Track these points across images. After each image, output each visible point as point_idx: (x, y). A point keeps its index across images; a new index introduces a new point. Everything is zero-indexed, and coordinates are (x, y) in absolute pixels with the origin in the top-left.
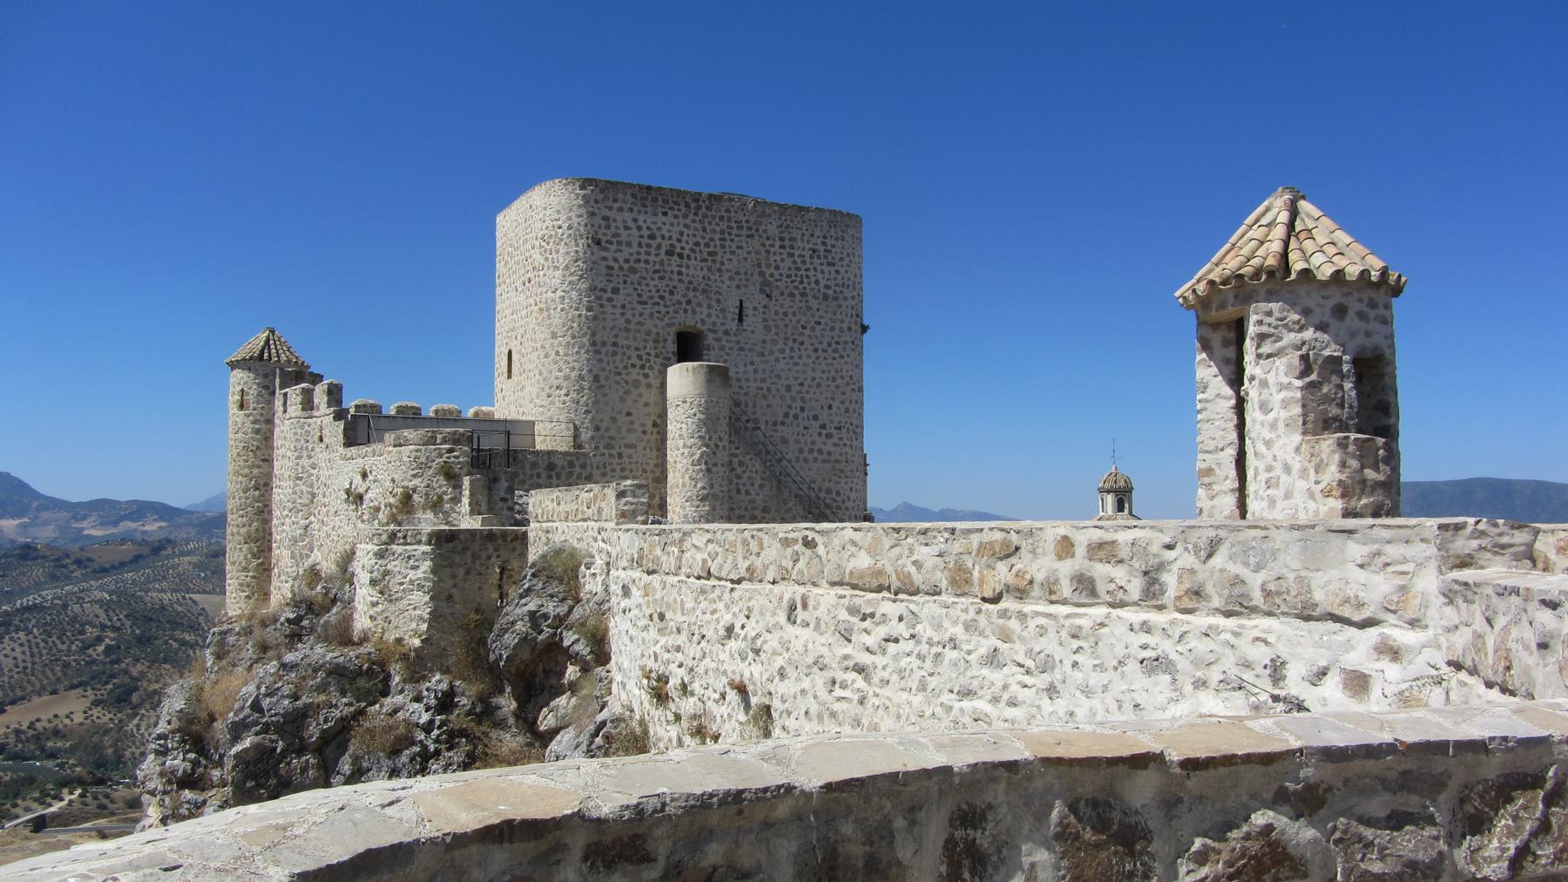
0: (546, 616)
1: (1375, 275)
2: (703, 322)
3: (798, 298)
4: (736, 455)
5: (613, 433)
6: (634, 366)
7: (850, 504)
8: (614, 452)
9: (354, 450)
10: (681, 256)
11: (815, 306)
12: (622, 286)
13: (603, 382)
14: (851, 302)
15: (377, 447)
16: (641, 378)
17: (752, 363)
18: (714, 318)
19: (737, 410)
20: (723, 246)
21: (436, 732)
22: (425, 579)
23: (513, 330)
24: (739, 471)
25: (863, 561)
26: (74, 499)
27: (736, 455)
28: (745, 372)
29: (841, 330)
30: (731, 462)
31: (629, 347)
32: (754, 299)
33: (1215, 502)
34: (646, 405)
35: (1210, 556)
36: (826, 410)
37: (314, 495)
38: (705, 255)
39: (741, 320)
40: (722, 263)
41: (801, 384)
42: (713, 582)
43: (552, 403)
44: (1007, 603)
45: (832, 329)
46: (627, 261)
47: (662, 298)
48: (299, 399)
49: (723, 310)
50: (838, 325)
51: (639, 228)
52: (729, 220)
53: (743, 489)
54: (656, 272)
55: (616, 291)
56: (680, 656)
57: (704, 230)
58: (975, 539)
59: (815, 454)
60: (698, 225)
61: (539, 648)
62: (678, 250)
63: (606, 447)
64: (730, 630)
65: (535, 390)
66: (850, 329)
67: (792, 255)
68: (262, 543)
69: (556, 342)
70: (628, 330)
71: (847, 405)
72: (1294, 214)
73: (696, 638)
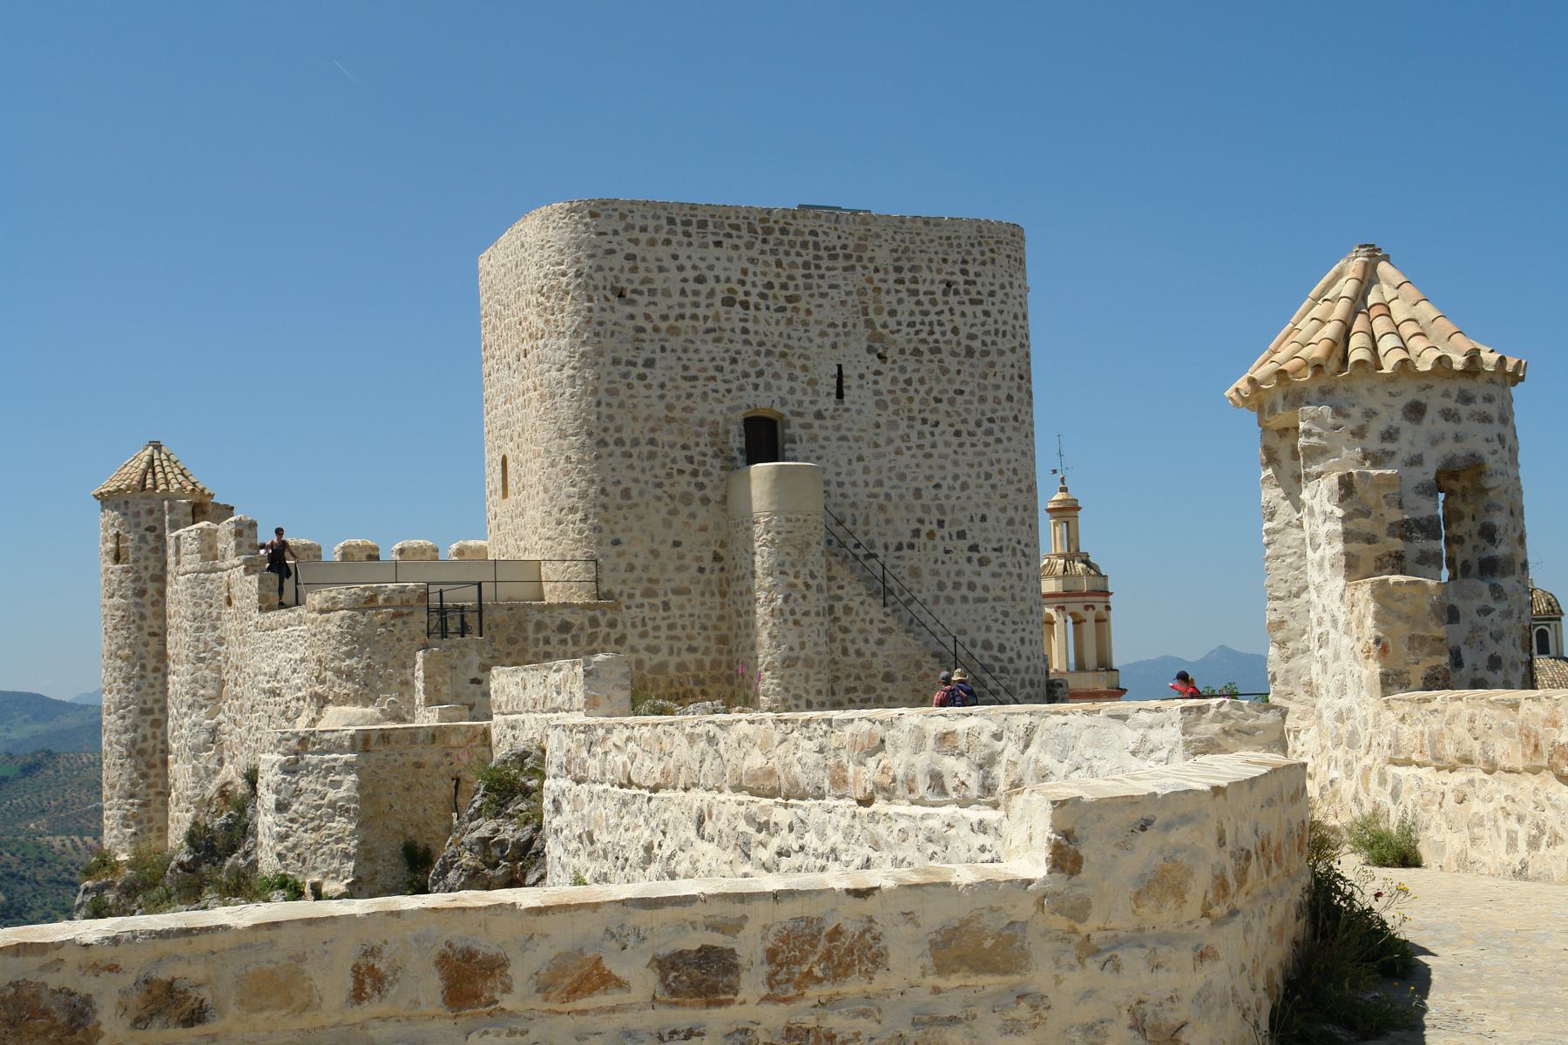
0: (502, 844)
1: (1459, 361)
2: (783, 402)
3: (927, 356)
4: (840, 598)
5: (654, 572)
6: (681, 472)
7: (1022, 664)
8: (658, 601)
10: (745, 305)
11: (953, 368)
12: (658, 355)
13: (636, 499)
14: (1010, 358)
16: (692, 489)
17: (860, 459)
18: (798, 396)
19: (839, 530)
20: (808, 287)
22: (349, 799)
23: (507, 426)
24: (845, 621)
25: (756, 761)
27: (840, 598)
28: (850, 473)
29: (997, 401)
30: (831, 608)
31: (672, 446)
32: (858, 361)
33: (1291, 664)
34: (703, 529)
35: (1027, 746)
36: (977, 524)
37: (223, 683)
38: (782, 302)
39: (840, 395)
41: (937, 486)
42: (634, 791)
43: (564, 533)
44: (880, 806)
45: (982, 400)
46: (665, 318)
47: (720, 369)
49: (812, 382)
50: (990, 394)
51: (681, 268)
52: (816, 246)
53: (852, 649)
54: (708, 331)
55: (649, 363)
57: (779, 264)
58: (849, 729)
59: (964, 591)
60: (771, 259)
62: (740, 297)
63: (643, 595)
64: (648, 848)
65: (539, 516)
66: (1010, 398)
67: (914, 293)
68: (150, 759)
69: (565, 443)
70: (670, 420)
71: (1011, 513)
72: (1368, 279)
73: (621, 861)
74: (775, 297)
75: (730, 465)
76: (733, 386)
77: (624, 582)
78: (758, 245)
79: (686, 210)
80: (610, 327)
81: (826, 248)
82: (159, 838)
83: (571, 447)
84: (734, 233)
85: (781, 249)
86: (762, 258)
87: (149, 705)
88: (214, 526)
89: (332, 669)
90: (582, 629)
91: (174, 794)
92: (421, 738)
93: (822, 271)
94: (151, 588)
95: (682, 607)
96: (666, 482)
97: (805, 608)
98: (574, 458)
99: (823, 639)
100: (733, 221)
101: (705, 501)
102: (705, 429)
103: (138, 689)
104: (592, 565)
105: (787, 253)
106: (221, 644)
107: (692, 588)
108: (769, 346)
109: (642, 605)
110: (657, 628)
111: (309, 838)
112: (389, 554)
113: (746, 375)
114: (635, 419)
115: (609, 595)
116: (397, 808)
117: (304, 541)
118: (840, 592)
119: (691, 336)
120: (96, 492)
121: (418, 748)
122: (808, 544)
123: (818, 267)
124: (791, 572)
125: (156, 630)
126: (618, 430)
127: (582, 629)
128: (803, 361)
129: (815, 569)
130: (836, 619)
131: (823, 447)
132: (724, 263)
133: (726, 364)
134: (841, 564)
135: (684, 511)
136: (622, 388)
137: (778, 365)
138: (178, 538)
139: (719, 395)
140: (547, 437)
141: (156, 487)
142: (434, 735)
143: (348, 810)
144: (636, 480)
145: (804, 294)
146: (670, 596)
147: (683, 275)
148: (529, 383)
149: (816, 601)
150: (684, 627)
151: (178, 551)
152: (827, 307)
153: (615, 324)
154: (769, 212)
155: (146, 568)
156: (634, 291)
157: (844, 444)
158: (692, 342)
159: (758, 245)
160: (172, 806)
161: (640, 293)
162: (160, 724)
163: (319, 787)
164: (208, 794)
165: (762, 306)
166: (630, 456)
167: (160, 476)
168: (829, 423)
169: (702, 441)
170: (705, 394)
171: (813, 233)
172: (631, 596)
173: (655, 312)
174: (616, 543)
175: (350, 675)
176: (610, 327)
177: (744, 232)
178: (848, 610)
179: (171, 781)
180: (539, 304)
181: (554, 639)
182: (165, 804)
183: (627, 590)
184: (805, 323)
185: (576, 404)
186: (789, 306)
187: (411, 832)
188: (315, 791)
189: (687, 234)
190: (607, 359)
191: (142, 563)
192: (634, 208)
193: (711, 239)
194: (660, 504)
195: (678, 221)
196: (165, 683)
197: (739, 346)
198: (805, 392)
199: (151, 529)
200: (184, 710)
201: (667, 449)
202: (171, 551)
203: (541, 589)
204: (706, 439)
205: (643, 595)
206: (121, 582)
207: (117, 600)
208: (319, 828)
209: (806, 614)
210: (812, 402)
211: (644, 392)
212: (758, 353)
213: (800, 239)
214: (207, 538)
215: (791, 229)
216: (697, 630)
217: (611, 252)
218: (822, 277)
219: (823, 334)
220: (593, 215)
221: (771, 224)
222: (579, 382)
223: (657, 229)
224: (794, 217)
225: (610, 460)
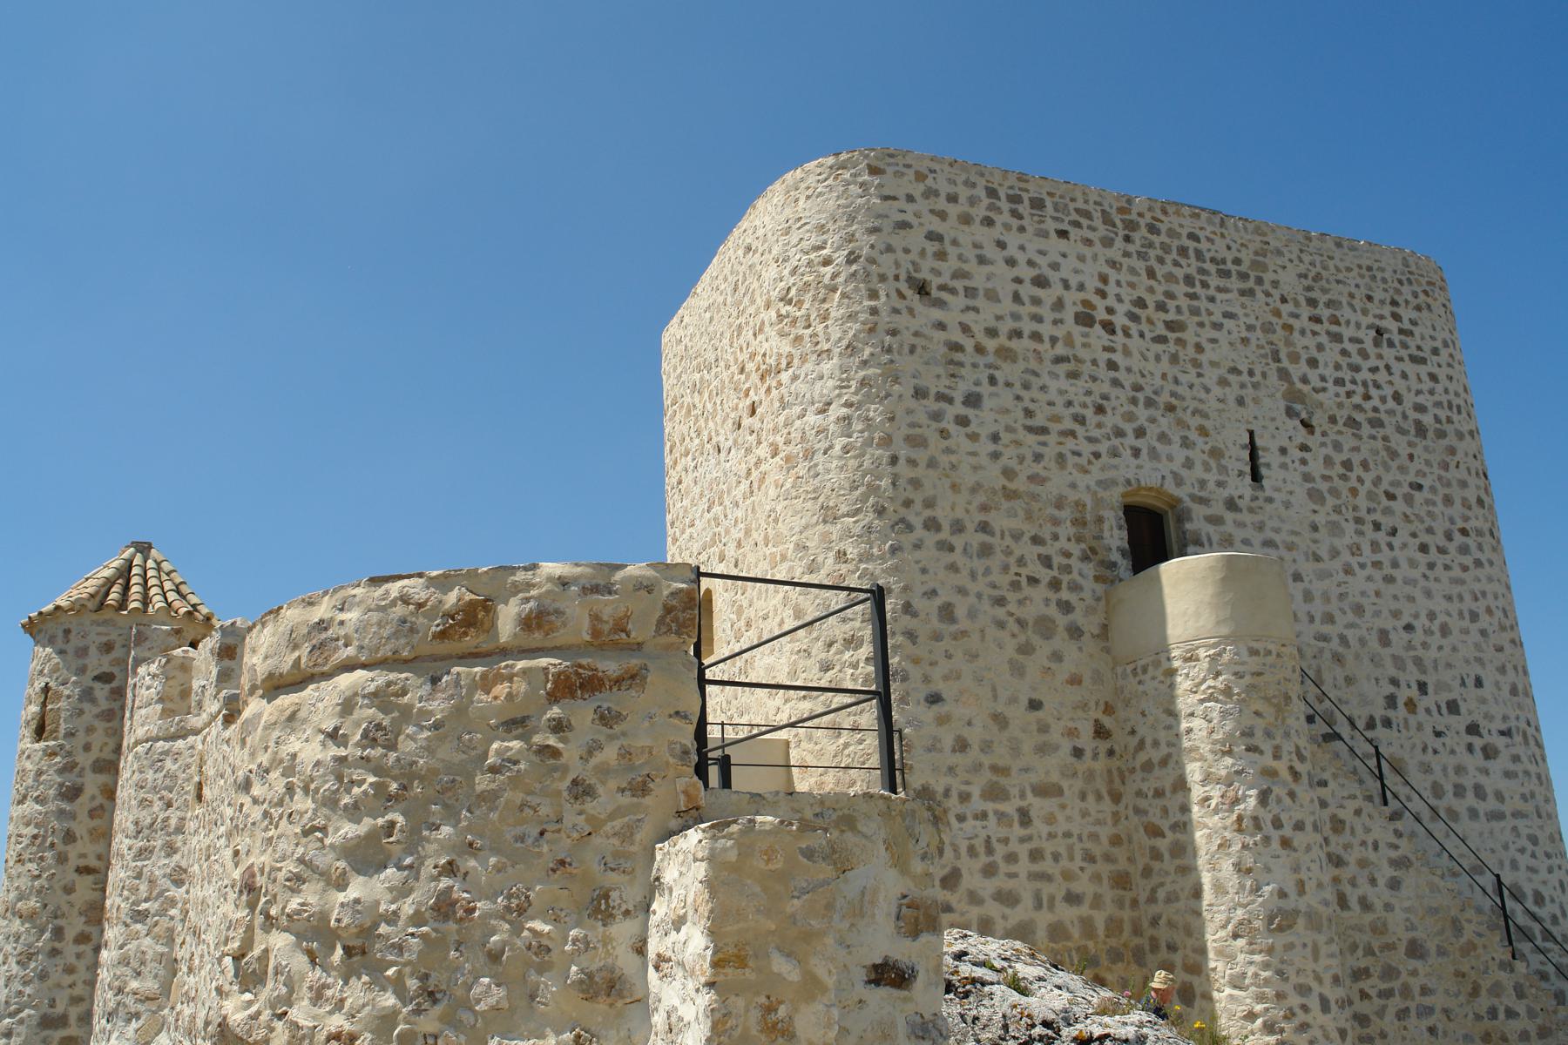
5: (1001, 756)
8: (1009, 808)
10: (1109, 327)
12: (985, 389)
13: (964, 624)
16: (1053, 611)
20: (1195, 312)
31: (1017, 536)
34: (1075, 680)
37: (172, 966)
38: (1161, 330)
46: (992, 333)
51: (1011, 262)
54: (1058, 360)
55: (973, 400)
57: (1151, 274)
62: (1101, 315)
69: (835, 530)
75: (1107, 575)
78: (1119, 243)
83: (847, 534)
85: (1152, 253)
86: (1126, 261)
87: (60, 1009)
94: (92, 784)
95: (1050, 819)
96: (1012, 597)
97: (1298, 816)
98: (852, 552)
100: (1080, 204)
101: (1075, 632)
102: (1066, 514)
103: (43, 976)
105: (1161, 260)
106: (178, 883)
107: (1065, 784)
109: (983, 816)
110: (1011, 858)
119: (1033, 365)
123: (1205, 285)
124: (1267, 747)
125: (93, 862)
126: (929, 503)
133: (1089, 413)
135: (1043, 649)
137: (1165, 423)
139: (1083, 461)
140: (798, 523)
144: (962, 591)
152: (1224, 342)
153: (916, 334)
156: (942, 288)
159: (1119, 243)
161: (953, 291)
166: (951, 549)
171: (1193, 237)
172: (965, 797)
173: (978, 323)
175: (359, 950)
183: (957, 786)
184: (1196, 364)
185: (853, 463)
186: (1171, 336)
189: (1016, 214)
190: (904, 389)
191: (82, 737)
192: (937, 167)
193: (1051, 226)
194: (1003, 635)
197: (1106, 388)
198: (1207, 469)
199: (105, 678)
201: (1008, 541)
204: (1067, 530)
206: (39, 773)
207: (30, 807)
209: (1299, 826)
211: (967, 445)
215: (1163, 228)
216: (1078, 862)
217: (904, 225)
221: (1134, 216)
222: (858, 426)
225: (918, 554)
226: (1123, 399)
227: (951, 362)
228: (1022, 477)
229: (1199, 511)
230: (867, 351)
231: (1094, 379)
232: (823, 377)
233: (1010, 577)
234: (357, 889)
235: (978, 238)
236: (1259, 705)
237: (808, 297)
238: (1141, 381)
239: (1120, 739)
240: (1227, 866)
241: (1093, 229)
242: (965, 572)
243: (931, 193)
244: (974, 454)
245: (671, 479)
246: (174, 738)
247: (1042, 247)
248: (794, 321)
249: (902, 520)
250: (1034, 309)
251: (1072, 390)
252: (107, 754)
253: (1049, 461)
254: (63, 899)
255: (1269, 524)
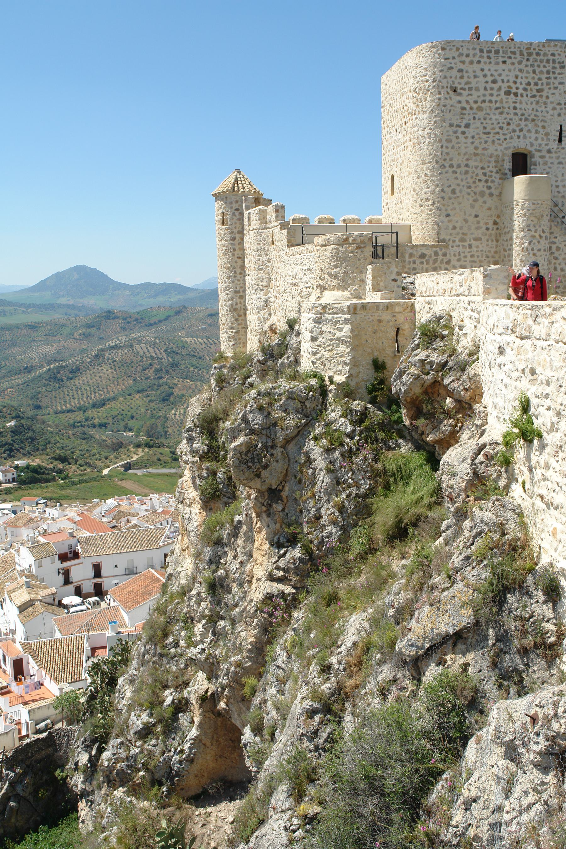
0: (431, 363)
2: (532, 144)
4: (555, 243)
5: (465, 230)
8: (466, 244)
9: (294, 249)
10: (516, 95)
12: (472, 121)
13: (458, 194)
15: (310, 247)
16: (485, 189)
20: (548, 84)
21: (357, 438)
22: (347, 337)
23: (395, 160)
24: (556, 254)
26: (131, 283)
27: (555, 243)
30: (550, 247)
31: (476, 167)
34: (489, 209)
37: (270, 280)
38: (534, 92)
39: (560, 140)
40: (547, 97)
43: (423, 211)
46: (476, 102)
48: (257, 217)
49: (547, 134)
51: (485, 76)
52: (554, 61)
53: (559, 268)
54: (497, 108)
55: (467, 126)
56: (548, 402)
57: (534, 72)
60: (530, 69)
61: (426, 384)
62: (514, 90)
63: (460, 241)
65: (410, 203)
68: (239, 312)
69: (425, 167)
74: (531, 90)
75: (504, 177)
76: (508, 137)
77: (451, 234)
78: (524, 62)
79: (489, 45)
80: (449, 107)
81: (559, 63)
82: (244, 347)
83: (428, 169)
84: (513, 56)
85: (536, 64)
86: (526, 69)
87: (238, 289)
88: (265, 208)
89: (327, 274)
90: (430, 257)
91: (249, 328)
92: (381, 307)
93: (556, 75)
94: (238, 236)
95: (477, 247)
96: (473, 186)
97: (539, 247)
98: (429, 174)
99: (546, 263)
100: (512, 50)
101: (491, 195)
102: (493, 159)
103: (233, 282)
104: (436, 226)
105: (539, 66)
106: (269, 262)
107: (483, 237)
108: (526, 115)
109: (459, 246)
110: (465, 257)
111: (327, 354)
112: (339, 221)
113: (514, 131)
114: (459, 154)
115: (443, 241)
116: (369, 341)
117: (302, 216)
118: (555, 240)
119: (488, 111)
120: (213, 193)
121: (380, 313)
122: (542, 216)
123: (554, 73)
124: (533, 230)
125: (240, 256)
126: (451, 160)
127: (430, 257)
128: (543, 123)
129: (544, 228)
130: (552, 253)
131: (550, 168)
132: (507, 72)
133: (505, 126)
134: (556, 226)
135: (481, 200)
136: (454, 139)
137: (531, 126)
138: (249, 213)
139: (501, 142)
140: (416, 164)
141: (239, 190)
142: (376, 306)
143: (346, 342)
144: (458, 185)
145: (545, 87)
146: (472, 241)
147: (486, 79)
148: (407, 138)
149: (544, 244)
150: (478, 257)
151: (249, 220)
152: (557, 95)
153: (452, 106)
154: (531, 44)
155: (235, 228)
156: (461, 89)
157: (561, 166)
158: (489, 114)
159: (524, 62)
160: (249, 333)
161: (464, 89)
162: (243, 297)
163: (332, 331)
164: (265, 329)
165: (525, 95)
166: (456, 173)
167: (240, 185)
168: (554, 155)
169: (491, 165)
170: (493, 141)
171: (553, 55)
172: (454, 241)
173: (471, 99)
174: (448, 215)
175: (336, 277)
176: (449, 107)
177: (518, 56)
178: (558, 249)
179: (248, 322)
180: (414, 97)
181: (418, 262)
182: (246, 332)
183: (452, 238)
184: (545, 103)
185: (431, 147)
186: (538, 94)
187: (376, 353)
188: (330, 332)
189: (489, 58)
190: (446, 124)
191: (234, 225)
192: (463, 44)
193: (501, 60)
194: (469, 197)
195: (485, 51)
196: (244, 279)
197: (511, 116)
198: (543, 140)
199: (237, 210)
200: (254, 291)
201: (474, 169)
202: (246, 220)
203: (411, 238)
204: (493, 164)
205: (460, 241)
206: (225, 234)
207: (223, 242)
208: (332, 350)
209: (539, 250)
210: (546, 145)
211: (464, 140)
212: (521, 120)
213: (546, 58)
214: (263, 213)
215: (542, 53)
216: (484, 258)
217: (451, 68)
218: (555, 78)
219: (554, 109)
220: (443, 49)
221: (532, 50)
222: (433, 136)
223: (474, 55)
224: (544, 46)
225: (446, 175)
226: (517, 119)
227: (462, 114)
228: (480, 149)
229: (537, 154)
230: (437, 112)
231: (508, 114)
232: (424, 119)
233: (473, 180)
234: (335, 270)
235: (475, 69)
236: (533, 218)
237: (421, 92)
238: (524, 112)
239: (501, 225)
240: (518, 260)
241: (515, 58)
242: (460, 179)
243: (461, 55)
244: (466, 143)
245: (383, 133)
246: (264, 229)
247: (496, 68)
248: (417, 99)
249: (443, 165)
250: (491, 92)
251: (500, 118)
252: (240, 229)
253: (490, 143)
254: (235, 264)
255: (562, 156)
